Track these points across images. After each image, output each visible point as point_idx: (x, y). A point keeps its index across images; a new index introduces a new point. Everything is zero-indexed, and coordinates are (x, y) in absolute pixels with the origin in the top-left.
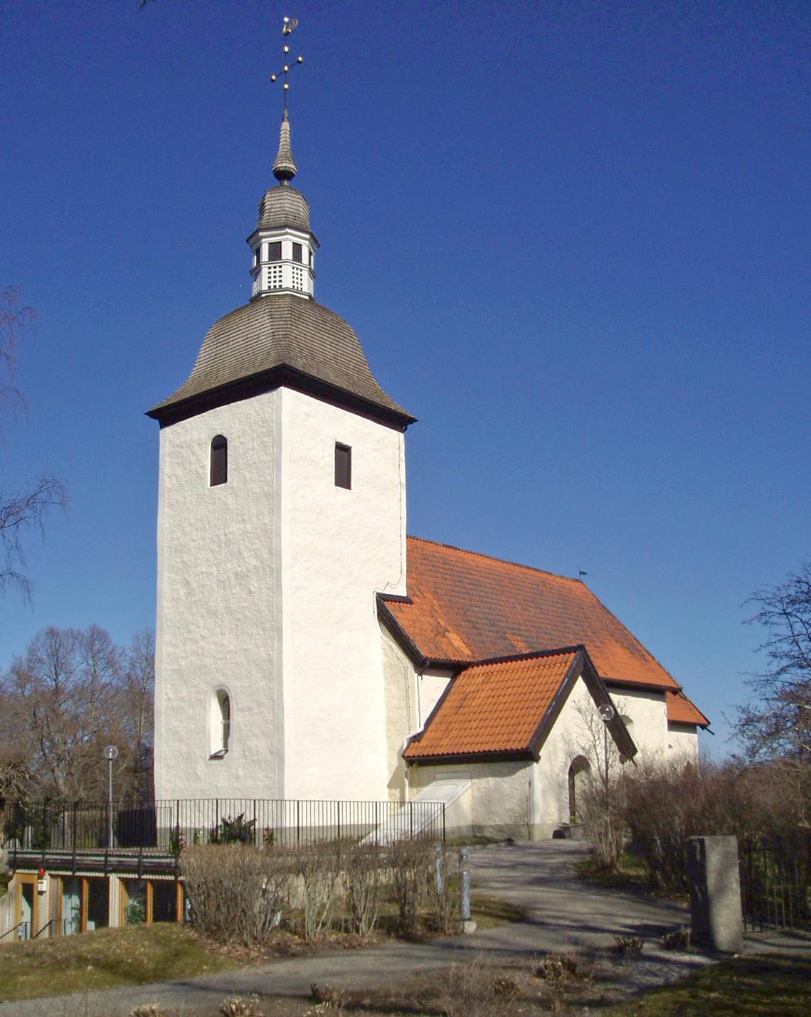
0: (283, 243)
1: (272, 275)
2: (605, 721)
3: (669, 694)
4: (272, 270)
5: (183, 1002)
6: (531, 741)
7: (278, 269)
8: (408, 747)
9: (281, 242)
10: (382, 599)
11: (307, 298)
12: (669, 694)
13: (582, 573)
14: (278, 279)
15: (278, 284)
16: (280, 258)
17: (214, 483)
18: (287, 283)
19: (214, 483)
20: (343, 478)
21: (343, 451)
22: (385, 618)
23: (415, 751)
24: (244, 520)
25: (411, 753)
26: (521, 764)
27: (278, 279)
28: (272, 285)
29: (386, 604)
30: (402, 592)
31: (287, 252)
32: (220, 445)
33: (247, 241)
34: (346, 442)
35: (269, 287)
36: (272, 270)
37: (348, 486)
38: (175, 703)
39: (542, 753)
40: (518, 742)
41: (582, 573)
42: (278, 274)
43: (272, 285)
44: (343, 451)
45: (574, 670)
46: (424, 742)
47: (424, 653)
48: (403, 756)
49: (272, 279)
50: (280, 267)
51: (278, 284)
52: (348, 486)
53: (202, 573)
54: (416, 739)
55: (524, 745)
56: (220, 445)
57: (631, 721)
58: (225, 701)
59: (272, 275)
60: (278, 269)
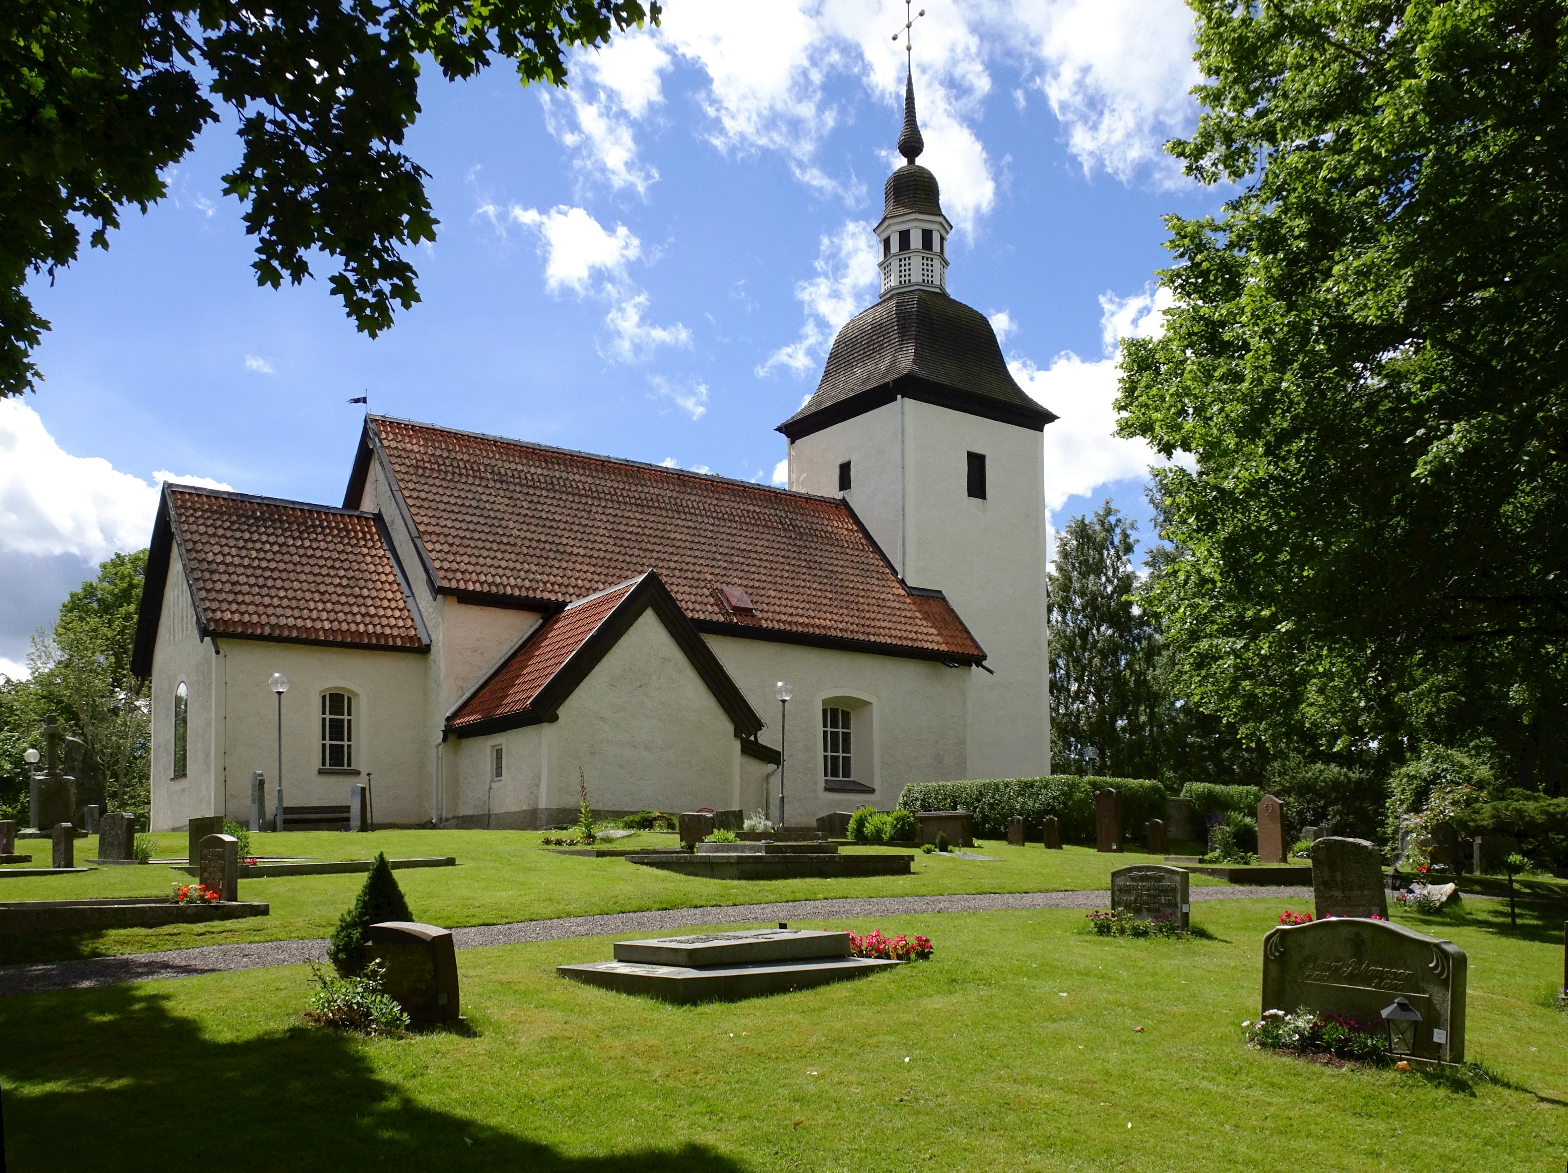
16: (909, 248)
31: (916, 241)
36: (903, 263)
37: (971, 456)
52: (971, 456)
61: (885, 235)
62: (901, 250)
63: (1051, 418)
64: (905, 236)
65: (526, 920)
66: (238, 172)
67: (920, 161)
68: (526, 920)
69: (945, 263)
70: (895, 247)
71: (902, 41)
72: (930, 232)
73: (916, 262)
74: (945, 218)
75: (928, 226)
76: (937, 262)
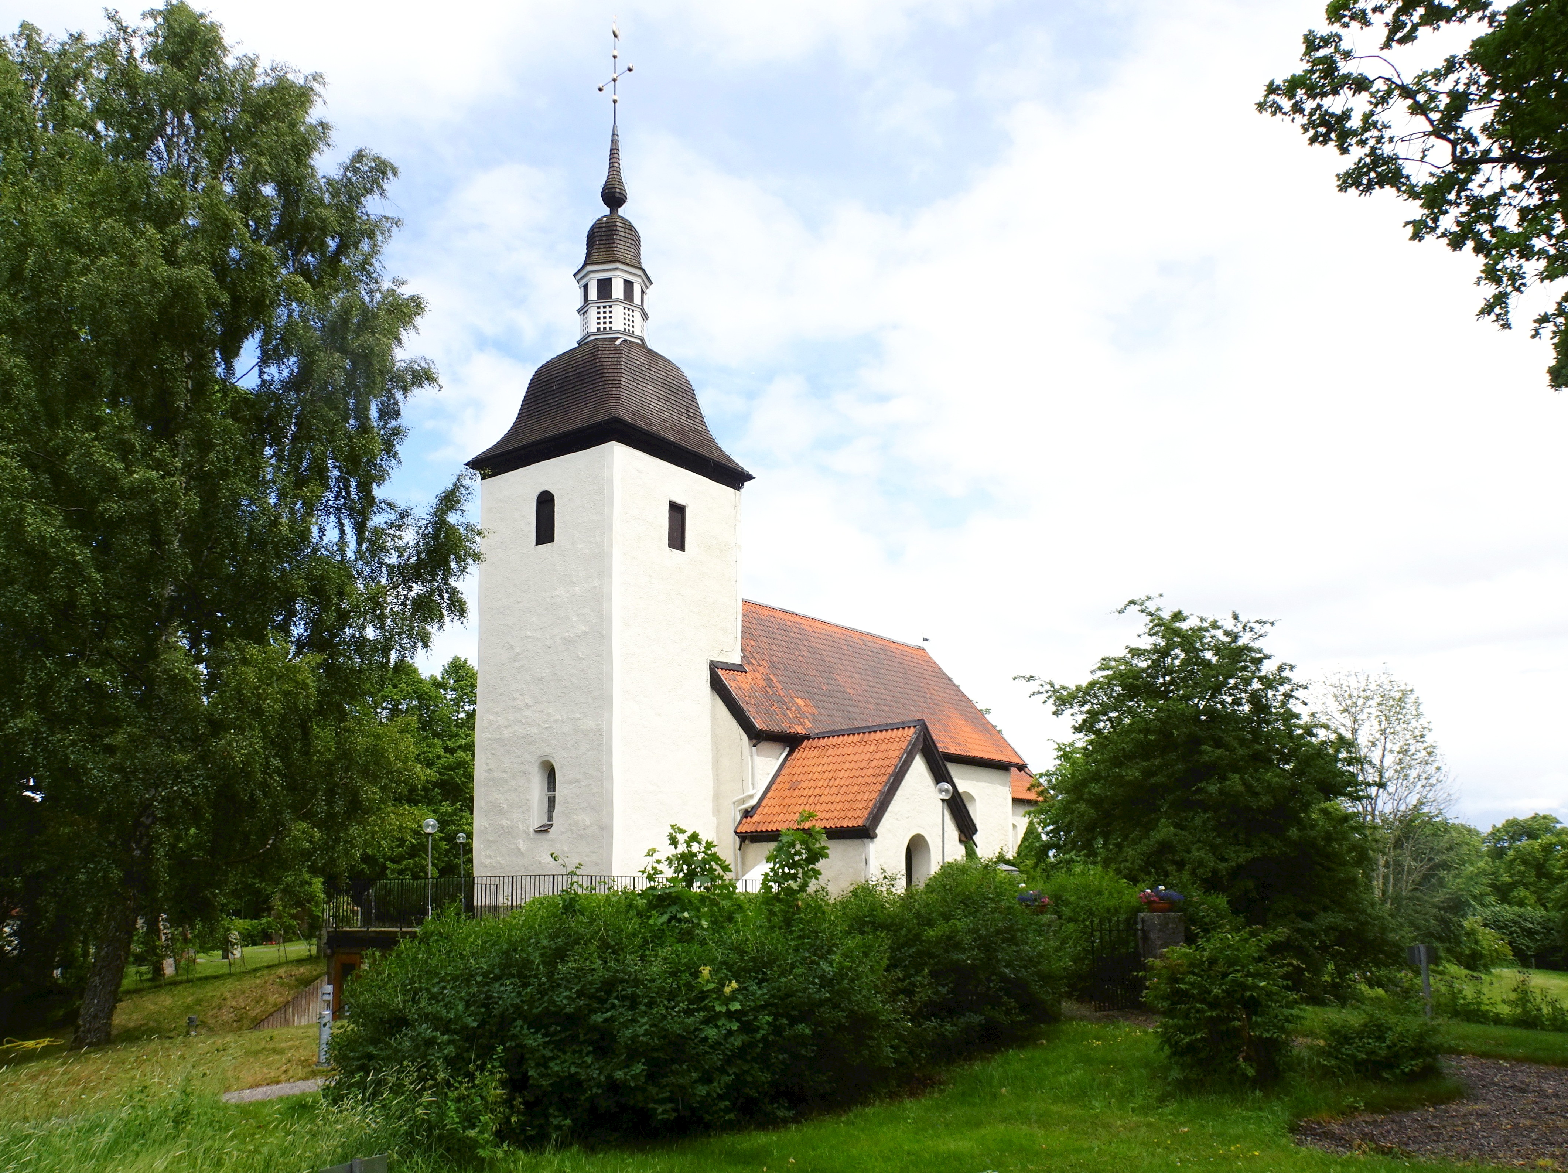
0: (613, 281)
1: (602, 315)
2: (943, 800)
3: (1014, 770)
4: (602, 310)
5: (1241, 708)
6: (868, 819)
7: (608, 309)
8: (740, 822)
9: (610, 279)
10: (714, 667)
11: (639, 341)
12: (1014, 770)
13: (926, 640)
14: (608, 320)
15: (608, 326)
16: (610, 296)
17: (539, 542)
18: (618, 325)
19: (539, 542)
20: (677, 540)
21: (677, 511)
22: (718, 686)
23: (748, 826)
24: (573, 583)
25: (743, 829)
26: (502, 450)
27: (608, 320)
28: (602, 326)
29: (720, 672)
30: (735, 658)
31: (618, 290)
32: (546, 502)
33: (575, 275)
34: (680, 501)
35: (599, 329)
36: (602, 310)
37: (682, 548)
38: (496, 774)
39: (878, 831)
40: (855, 819)
41: (926, 640)
42: (608, 315)
43: (602, 326)
44: (677, 511)
45: (914, 746)
46: (756, 818)
47: (759, 724)
48: (736, 832)
49: (602, 321)
50: (610, 307)
51: (608, 326)
52: (682, 548)
53: (527, 637)
54: (747, 814)
55: (860, 822)
56: (546, 502)
57: (972, 798)
58: (550, 773)
59: (602, 315)
60: (608, 309)
61: (583, 282)
62: (599, 298)
63: (749, 477)
64: (605, 287)
65: (181, 982)
66: (1081, 740)
67: (621, 211)
68: (181, 982)
69: (645, 316)
70: (593, 294)
71: (622, 66)
72: (632, 283)
73: (618, 311)
74: (644, 271)
75: (629, 278)
76: (638, 314)
